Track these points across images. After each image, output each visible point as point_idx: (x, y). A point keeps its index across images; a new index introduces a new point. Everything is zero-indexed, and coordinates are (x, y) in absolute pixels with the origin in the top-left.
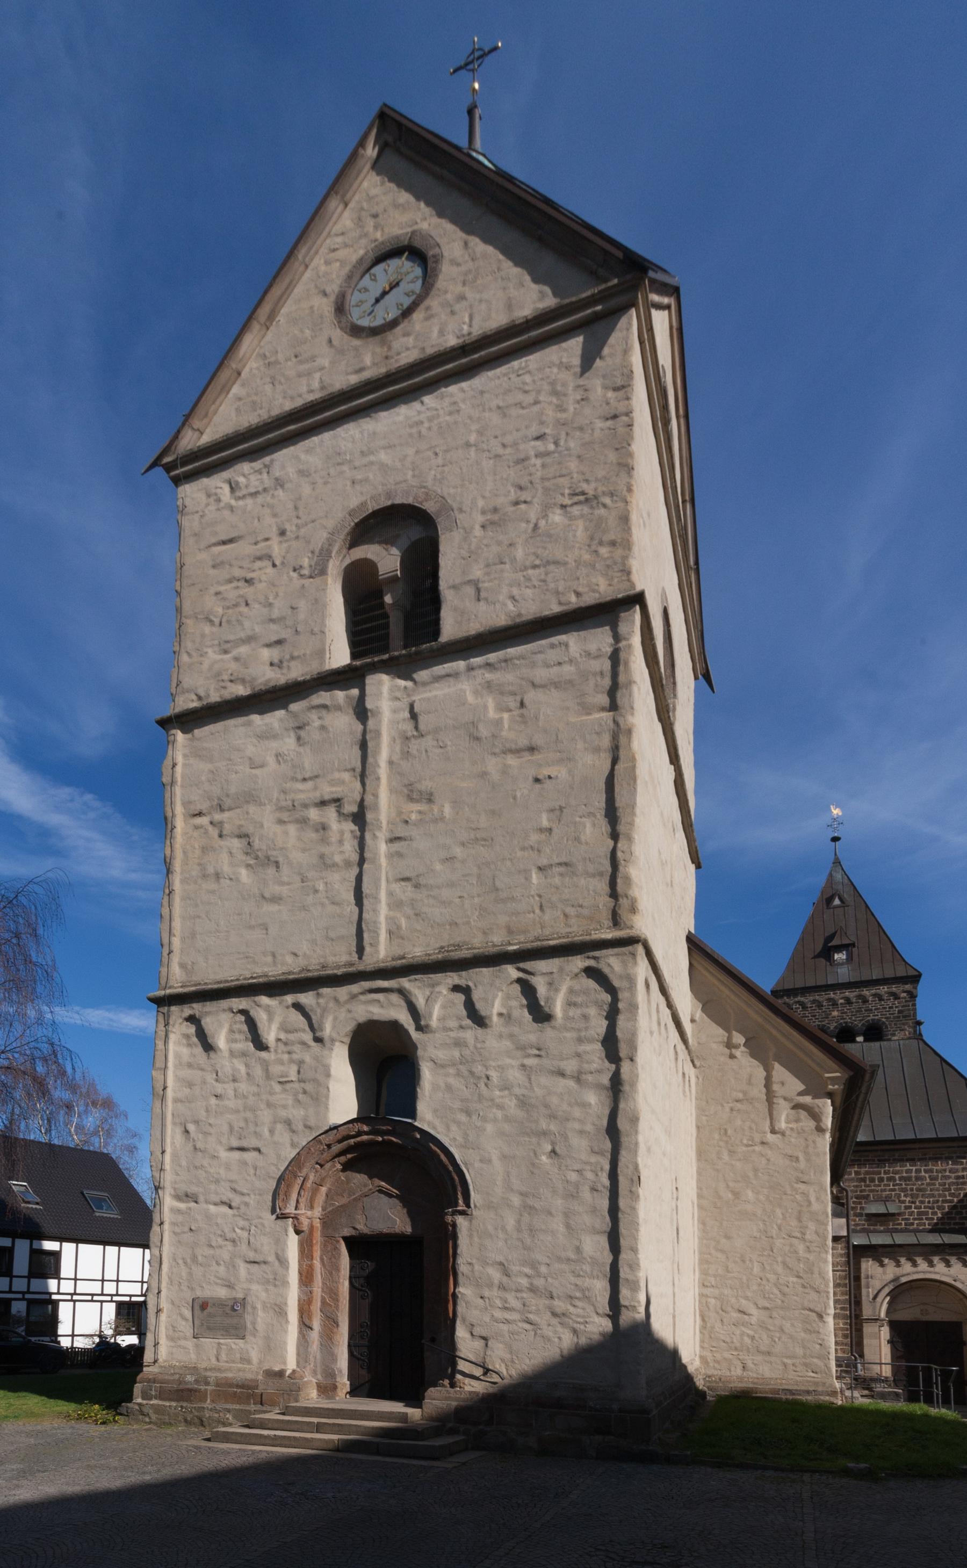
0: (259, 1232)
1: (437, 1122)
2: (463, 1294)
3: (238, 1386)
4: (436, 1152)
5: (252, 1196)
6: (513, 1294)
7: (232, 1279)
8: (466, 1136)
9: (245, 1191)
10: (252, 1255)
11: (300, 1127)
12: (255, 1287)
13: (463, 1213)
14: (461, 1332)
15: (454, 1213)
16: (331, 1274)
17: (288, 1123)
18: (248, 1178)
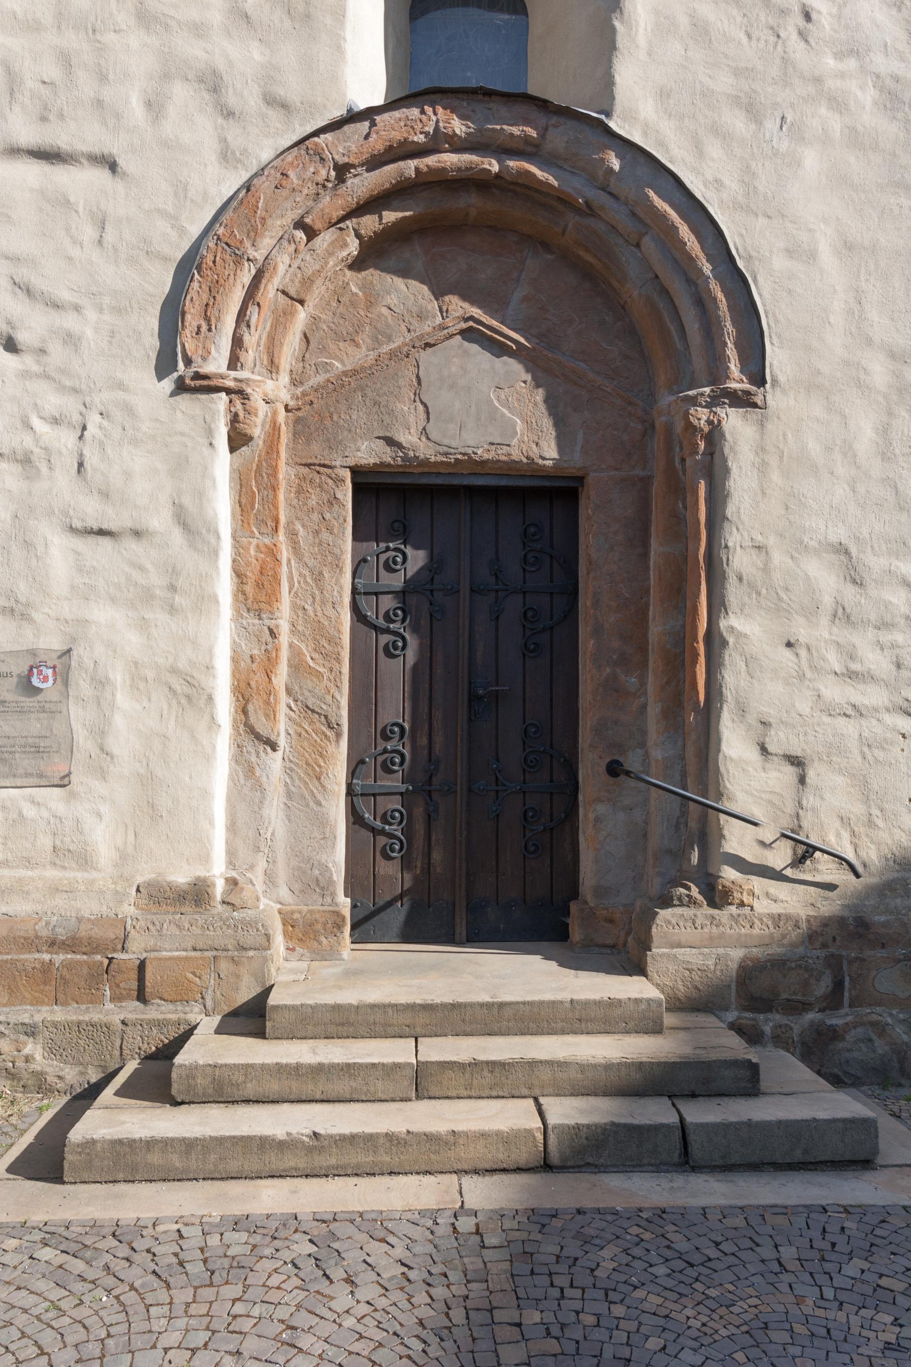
0: (116, 433)
1: (667, 128)
2: (740, 635)
3: (53, 944)
4: (664, 217)
5: (91, 314)
6: (871, 633)
7: (22, 589)
8: (748, 175)
9: (65, 295)
10: (92, 511)
11: (253, 101)
12: (101, 614)
13: (742, 401)
14: (734, 744)
15: (713, 402)
16: (318, 578)
17: (212, 83)
18: (75, 252)
